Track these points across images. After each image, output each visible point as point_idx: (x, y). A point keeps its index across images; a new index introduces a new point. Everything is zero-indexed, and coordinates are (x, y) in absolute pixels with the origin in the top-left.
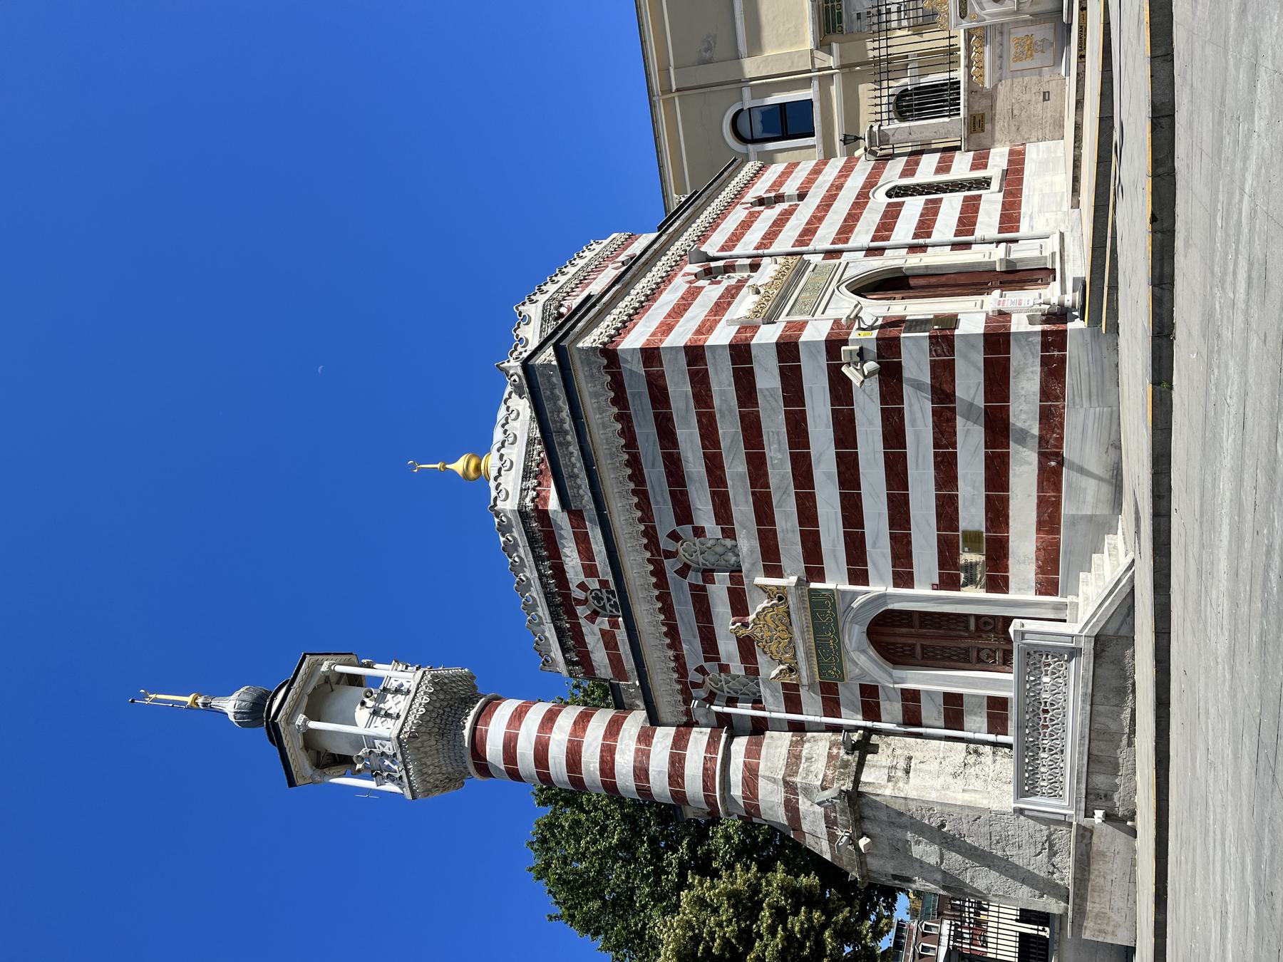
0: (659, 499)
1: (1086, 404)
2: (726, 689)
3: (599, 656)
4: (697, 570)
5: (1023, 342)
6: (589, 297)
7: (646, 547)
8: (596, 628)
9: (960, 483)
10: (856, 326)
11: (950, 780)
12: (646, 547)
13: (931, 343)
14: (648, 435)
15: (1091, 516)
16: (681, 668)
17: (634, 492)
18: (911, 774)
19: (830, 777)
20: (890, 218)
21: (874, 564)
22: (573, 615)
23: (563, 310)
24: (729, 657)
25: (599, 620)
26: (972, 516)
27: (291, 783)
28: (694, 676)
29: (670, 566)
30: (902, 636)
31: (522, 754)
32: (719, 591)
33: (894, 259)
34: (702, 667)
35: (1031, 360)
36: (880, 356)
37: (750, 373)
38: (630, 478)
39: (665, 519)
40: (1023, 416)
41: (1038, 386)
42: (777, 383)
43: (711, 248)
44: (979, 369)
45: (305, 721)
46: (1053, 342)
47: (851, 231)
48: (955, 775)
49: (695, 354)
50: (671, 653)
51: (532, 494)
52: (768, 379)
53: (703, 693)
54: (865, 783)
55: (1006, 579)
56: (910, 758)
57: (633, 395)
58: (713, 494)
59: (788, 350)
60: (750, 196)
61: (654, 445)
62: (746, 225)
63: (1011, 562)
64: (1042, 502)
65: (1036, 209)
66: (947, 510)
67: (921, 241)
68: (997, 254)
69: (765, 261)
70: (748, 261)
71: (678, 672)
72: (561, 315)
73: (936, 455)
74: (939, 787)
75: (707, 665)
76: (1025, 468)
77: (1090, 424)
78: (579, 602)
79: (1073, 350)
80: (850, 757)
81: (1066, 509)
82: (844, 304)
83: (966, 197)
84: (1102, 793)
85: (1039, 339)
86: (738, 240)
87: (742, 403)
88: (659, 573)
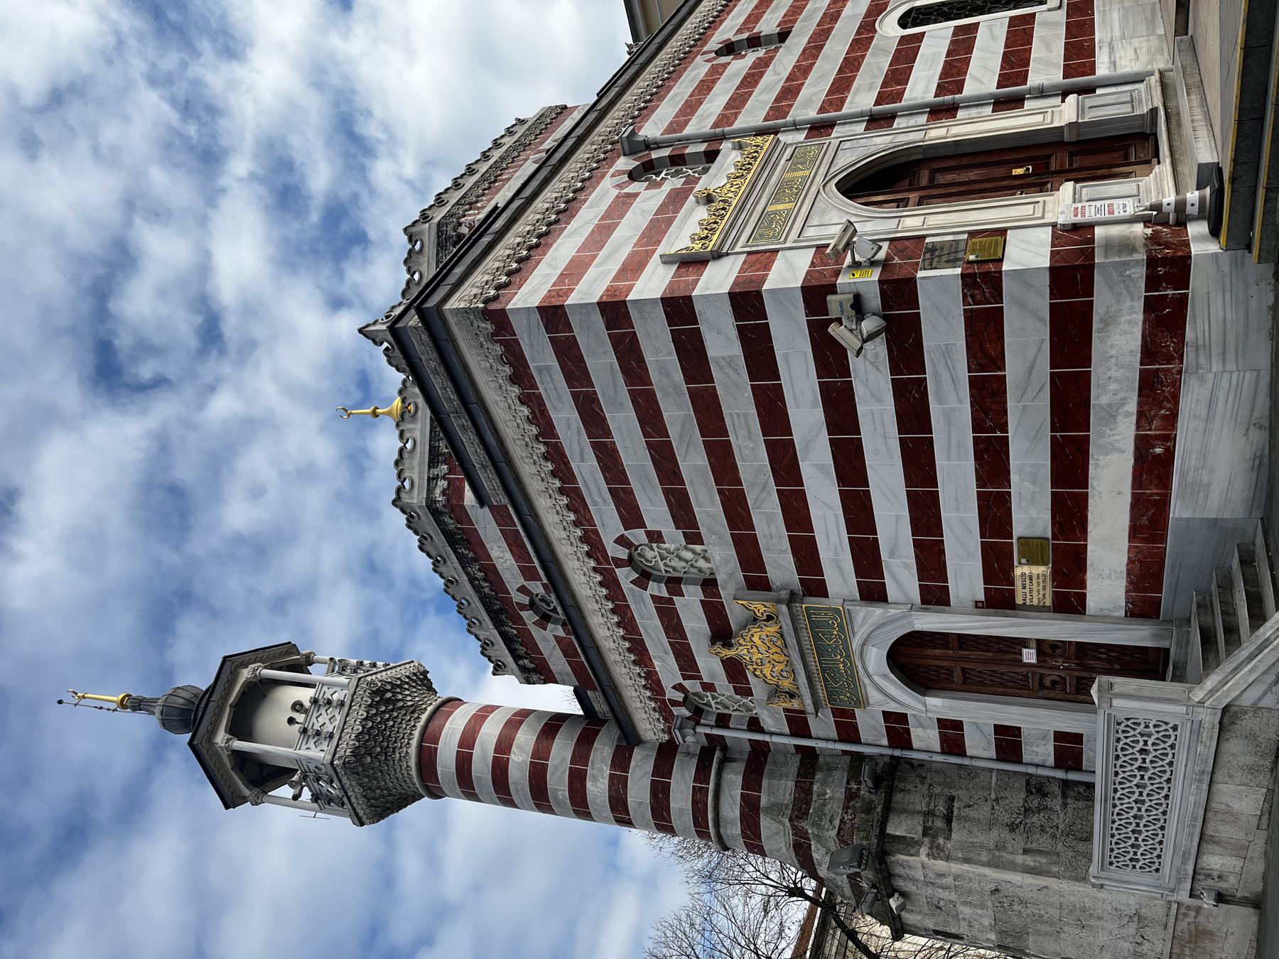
0: (597, 498)
1: (1216, 367)
4: (658, 580)
5: (1115, 276)
6: (496, 208)
7: (589, 554)
9: (1014, 478)
10: (848, 260)
11: (1005, 834)
12: (589, 554)
13: (965, 286)
15: (1215, 521)
17: (561, 491)
18: (954, 825)
20: (907, 53)
21: (893, 577)
23: (464, 230)
24: (712, 675)
25: (550, 626)
26: (1031, 513)
28: (671, 694)
31: (479, 778)
32: (690, 606)
33: (911, 133)
35: (1128, 303)
36: (886, 303)
37: (697, 336)
38: (554, 474)
39: (609, 524)
40: (1113, 386)
41: (1139, 342)
42: (736, 350)
43: (651, 129)
44: (1041, 320)
45: (228, 740)
46: (1168, 270)
47: (848, 88)
48: (1012, 828)
49: (614, 311)
51: (442, 484)
52: (722, 343)
56: (952, 799)
58: (667, 493)
59: (747, 303)
60: (714, 42)
61: (579, 433)
62: (705, 87)
63: (1090, 576)
64: (1138, 503)
65: (1117, 33)
66: (994, 513)
68: (1065, 113)
69: (725, 146)
70: (702, 148)
71: (651, 690)
72: (460, 236)
74: (992, 846)
75: (687, 684)
76: (1114, 457)
77: (1221, 396)
79: (1200, 283)
80: (873, 797)
81: (1178, 510)
82: (832, 216)
83: (1012, 18)
84: (1215, 874)
86: (692, 113)
88: (610, 583)
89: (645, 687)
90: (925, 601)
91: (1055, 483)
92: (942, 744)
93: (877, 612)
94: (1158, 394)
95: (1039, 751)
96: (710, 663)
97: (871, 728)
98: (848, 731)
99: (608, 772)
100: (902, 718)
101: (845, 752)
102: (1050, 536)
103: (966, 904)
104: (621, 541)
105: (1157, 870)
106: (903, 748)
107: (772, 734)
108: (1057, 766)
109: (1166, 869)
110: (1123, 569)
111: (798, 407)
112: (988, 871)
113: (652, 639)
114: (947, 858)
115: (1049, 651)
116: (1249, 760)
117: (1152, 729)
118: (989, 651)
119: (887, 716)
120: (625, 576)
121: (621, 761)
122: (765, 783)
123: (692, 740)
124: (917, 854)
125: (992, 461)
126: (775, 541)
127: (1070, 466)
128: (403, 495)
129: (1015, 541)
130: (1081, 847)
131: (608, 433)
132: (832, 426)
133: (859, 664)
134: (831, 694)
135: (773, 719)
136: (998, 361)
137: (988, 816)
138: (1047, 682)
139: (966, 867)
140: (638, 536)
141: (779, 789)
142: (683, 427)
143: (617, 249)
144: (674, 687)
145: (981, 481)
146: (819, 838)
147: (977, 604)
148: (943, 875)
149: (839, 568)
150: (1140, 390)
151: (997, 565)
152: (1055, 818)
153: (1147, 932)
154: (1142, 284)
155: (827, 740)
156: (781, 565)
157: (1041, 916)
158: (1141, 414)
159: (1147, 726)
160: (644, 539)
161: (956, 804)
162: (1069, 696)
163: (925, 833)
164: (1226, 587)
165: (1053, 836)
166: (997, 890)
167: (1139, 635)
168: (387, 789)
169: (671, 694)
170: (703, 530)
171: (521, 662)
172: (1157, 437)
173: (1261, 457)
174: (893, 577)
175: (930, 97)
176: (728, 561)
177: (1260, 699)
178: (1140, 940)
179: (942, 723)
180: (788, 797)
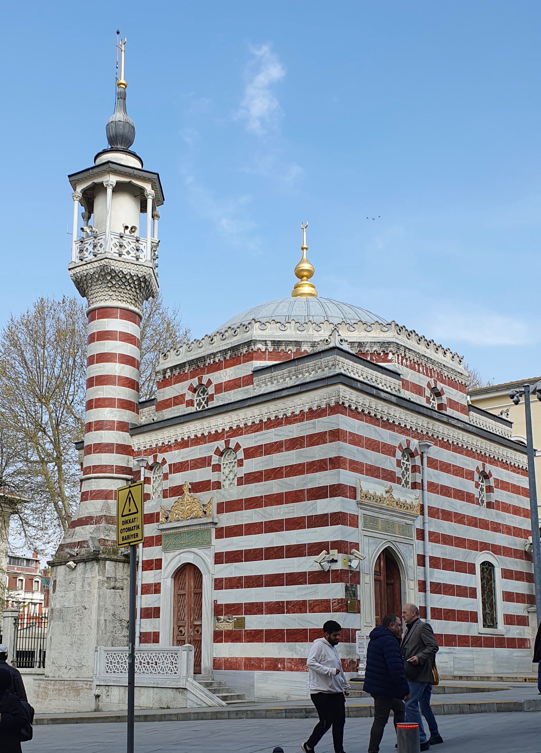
0: (258, 438)
3: (170, 392)
8: (186, 391)
11: (111, 612)
15: (254, 686)
18: (113, 590)
19: (107, 544)
21: (226, 567)
25: (191, 393)
26: (253, 622)
27: (69, 176)
30: (189, 583)
32: (203, 474)
34: (166, 462)
39: (247, 441)
40: (302, 650)
48: (114, 615)
54: (105, 564)
55: (221, 641)
56: (122, 589)
57: (314, 423)
60: (489, 468)
63: (230, 644)
64: (260, 660)
65: (457, 656)
66: (255, 608)
73: (283, 602)
74: (106, 606)
75: (167, 466)
80: (120, 554)
81: (257, 673)
84: (109, 694)
87: (310, 491)
88: (216, 436)
90: (216, 580)
93: (210, 560)
99: (116, 420)
102: (246, 629)
103: (75, 595)
104: (238, 446)
105: (107, 672)
109: (108, 675)
112: (95, 606)
113: (189, 452)
114: (99, 588)
115: (196, 629)
116: (165, 700)
118: (194, 605)
120: (221, 444)
124: (99, 575)
125: (277, 608)
126: (240, 518)
127: (274, 636)
129: (243, 616)
130: (109, 643)
131: (287, 449)
132: (289, 548)
133: (185, 550)
134: (167, 535)
136: (312, 611)
137: (118, 605)
138: (181, 629)
139: (96, 596)
140: (240, 455)
142: (289, 485)
145: (267, 604)
146: (98, 529)
147: (215, 601)
148: (89, 584)
149: (229, 545)
150: (301, 659)
151: (233, 609)
152: (119, 632)
153: (74, 671)
156: (228, 520)
157: (74, 627)
158: (292, 659)
159: (175, 664)
160: (239, 458)
162: (175, 637)
164: (228, 691)
165: (112, 632)
166: (86, 608)
167: (206, 663)
168: (91, 286)
169: (160, 457)
172: (284, 665)
173: (277, 699)
176: (230, 496)
177: (190, 700)
178: (68, 668)
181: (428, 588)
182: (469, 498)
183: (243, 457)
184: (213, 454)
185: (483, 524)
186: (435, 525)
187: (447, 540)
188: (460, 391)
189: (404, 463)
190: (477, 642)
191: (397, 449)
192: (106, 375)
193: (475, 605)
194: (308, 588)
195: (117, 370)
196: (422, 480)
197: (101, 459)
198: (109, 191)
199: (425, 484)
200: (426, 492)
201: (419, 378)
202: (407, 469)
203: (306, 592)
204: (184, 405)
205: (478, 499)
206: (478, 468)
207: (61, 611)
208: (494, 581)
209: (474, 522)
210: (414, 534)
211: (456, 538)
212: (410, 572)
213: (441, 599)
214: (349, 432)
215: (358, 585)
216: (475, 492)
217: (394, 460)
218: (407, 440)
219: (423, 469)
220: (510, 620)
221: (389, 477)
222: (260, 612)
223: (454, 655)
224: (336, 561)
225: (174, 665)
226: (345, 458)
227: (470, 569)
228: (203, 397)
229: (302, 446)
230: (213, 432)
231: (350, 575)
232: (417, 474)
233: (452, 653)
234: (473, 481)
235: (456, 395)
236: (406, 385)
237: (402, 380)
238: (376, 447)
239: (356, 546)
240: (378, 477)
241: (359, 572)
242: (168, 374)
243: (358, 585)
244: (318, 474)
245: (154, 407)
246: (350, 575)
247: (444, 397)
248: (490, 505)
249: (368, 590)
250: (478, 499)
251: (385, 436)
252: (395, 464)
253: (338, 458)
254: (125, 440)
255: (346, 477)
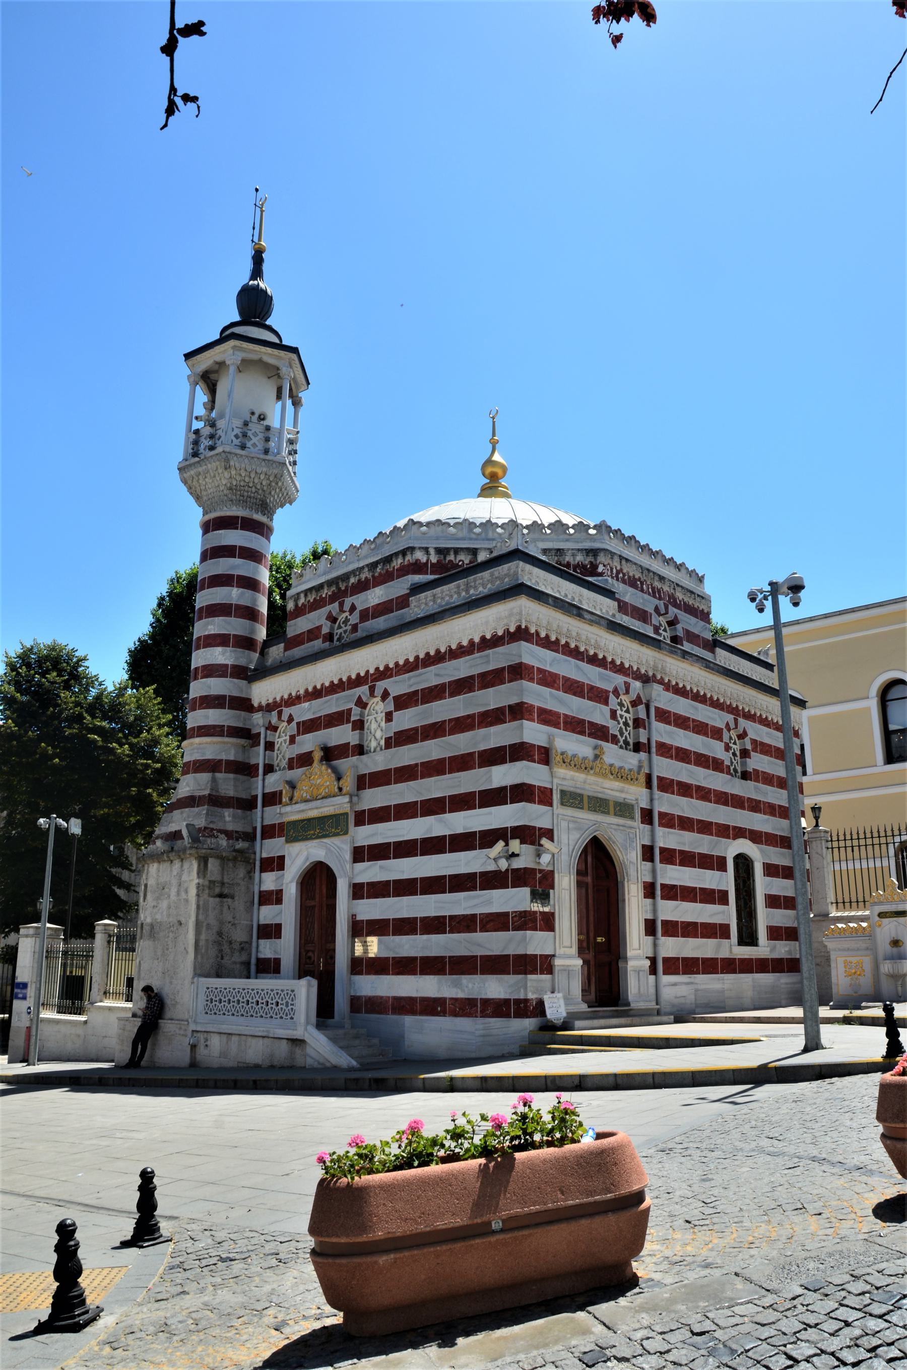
2: (280, 740)
9: (425, 937)
11: (215, 929)
14: (459, 670)
16: (292, 701)
18: (218, 899)
21: (371, 866)
22: (333, 598)
25: (329, 623)
27: (188, 356)
28: (287, 712)
29: (363, 690)
32: (341, 735)
39: (398, 686)
40: (470, 985)
44: (503, 951)
50: (302, 692)
53: (274, 721)
58: (416, 729)
64: (411, 1000)
67: (658, 892)
71: (289, 699)
75: (294, 724)
78: (341, 605)
81: (409, 1020)
84: (208, 1043)
85: (522, 997)
87: (482, 753)
88: (359, 681)
89: (290, 694)
90: (355, 848)
91: (422, 958)
92: (266, 891)
93: (348, 856)
94: (466, 1007)
95: (267, 949)
96: (309, 742)
97: (271, 848)
98: (269, 832)
100: (281, 867)
101: (255, 829)
106: (261, 867)
107: (264, 780)
108: (258, 960)
110: (377, 994)
111: (464, 818)
114: (198, 895)
117: (290, 1007)
119: (282, 859)
121: (239, 672)
122: (231, 776)
123: (258, 721)
128: (416, 526)
131: (452, 695)
135: (273, 782)
136: (484, 929)
138: (310, 954)
141: (228, 785)
143: (561, 702)
144: (291, 715)
145: (423, 919)
147: (354, 916)
148: (186, 891)
154: (516, 997)
155: (262, 818)
156: (375, 798)
157: (168, 949)
161: (229, 900)
163: (212, 882)
166: (181, 924)
170: (393, 750)
171: (302, 595)
174: (371, 866)
175: (660, 881)
179: (279, 893)
180: (223, 792)
181: (658, 892)
182: (717, 765)
183: (393, 709)
184: (354, 706)
185: (738, 802)
186: (667, 803)
187: (686, 824)
188: (702, 620)
189: (621, 716)
190: (730, 966)
191: (611, 694)
192: (219, 604)
193: (728, 914)
194: (479, 896)
195: (234, 596)
196: (649, 740)
197: (207, 717)
198: (232, 369)
199: (653, 745)
200: (654, 756)
201: (643, 599)
202: (626, 724)
203: (475, 901)
204: (321, 640)
205: (728, 767)
206: (727, 724)
207: (152, 926)
208: (754, 881)
209: (723, 799)
210: (638, 815)
211: (699, 821)
212: (632, 872)
213: (677, 907)
214: (538, 668)
215: (551, 891)
216: (726, 757)
217: (606, 710)
218: (625, 683)
219: (649, 723)
220: (775, 933)
221: (599, 734)
222: (413, 931)
223: (696, 986)
224: (518, 855)
225: (290, 1007)
226: (532, 706)
227: (719, 864)
228: (345, 628)
229: (471, 690)
230: (354, 677)
231: (538, 875)
232: (641, 730)
233: (692, 983)
234: (722, 741)
235: (695, 624)
236: (623, 607)
237: (619, 601)
238: (579, 690)
239: (549, 834)
240: (582, 733)
241: (552, 872)
242: (302, 600)
243: (551, 891)
244: (493, 729)
245: (282, 645)
246: (538, 875)
247: (679, 627)
248: (745, 776)
249: (567, 897)
250: (728, 767)
251: (591, 675)
252: (608, 715)
253: (521, 705)
254: (242, 691)
255: (533, 732)
